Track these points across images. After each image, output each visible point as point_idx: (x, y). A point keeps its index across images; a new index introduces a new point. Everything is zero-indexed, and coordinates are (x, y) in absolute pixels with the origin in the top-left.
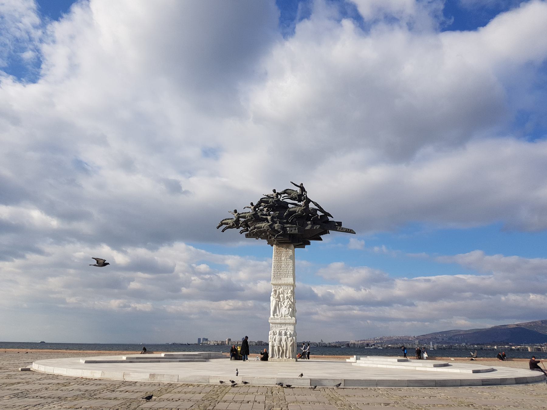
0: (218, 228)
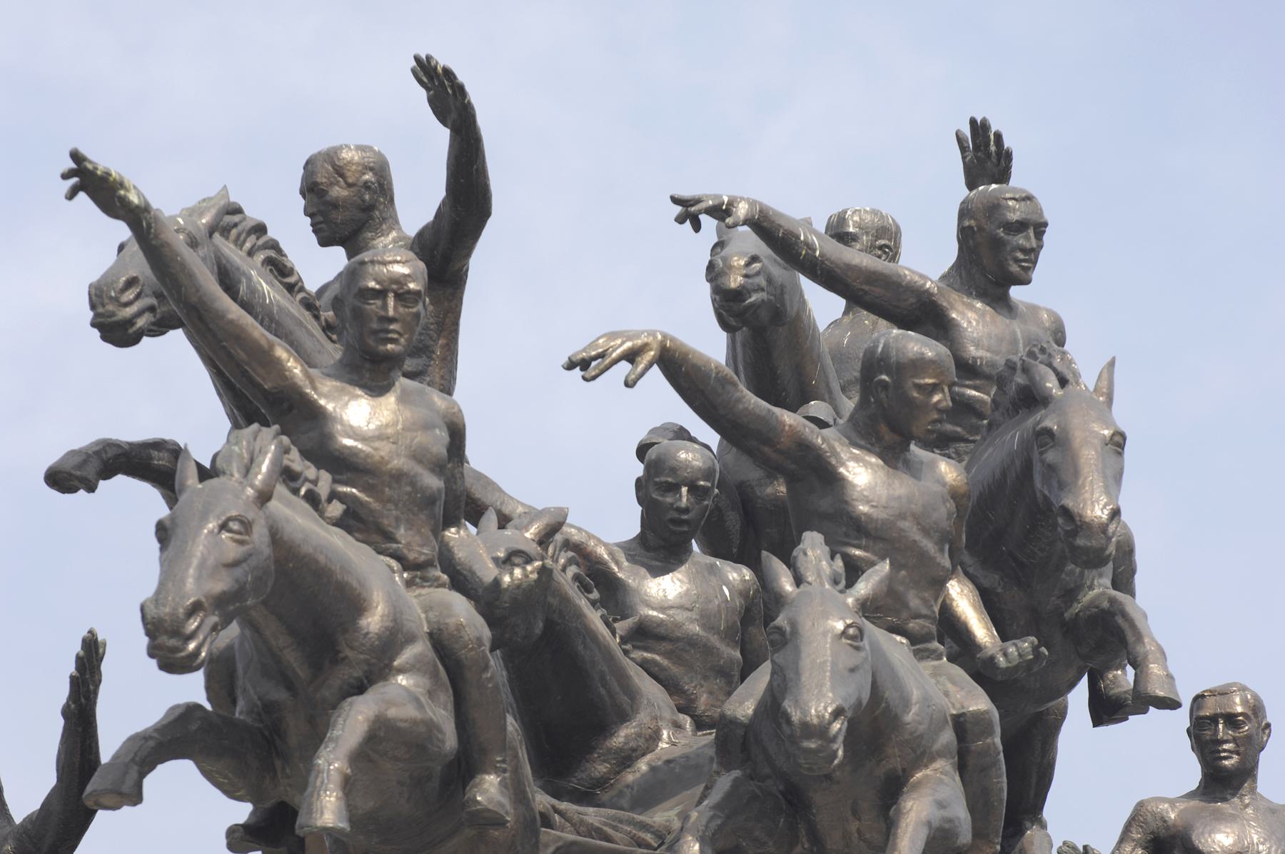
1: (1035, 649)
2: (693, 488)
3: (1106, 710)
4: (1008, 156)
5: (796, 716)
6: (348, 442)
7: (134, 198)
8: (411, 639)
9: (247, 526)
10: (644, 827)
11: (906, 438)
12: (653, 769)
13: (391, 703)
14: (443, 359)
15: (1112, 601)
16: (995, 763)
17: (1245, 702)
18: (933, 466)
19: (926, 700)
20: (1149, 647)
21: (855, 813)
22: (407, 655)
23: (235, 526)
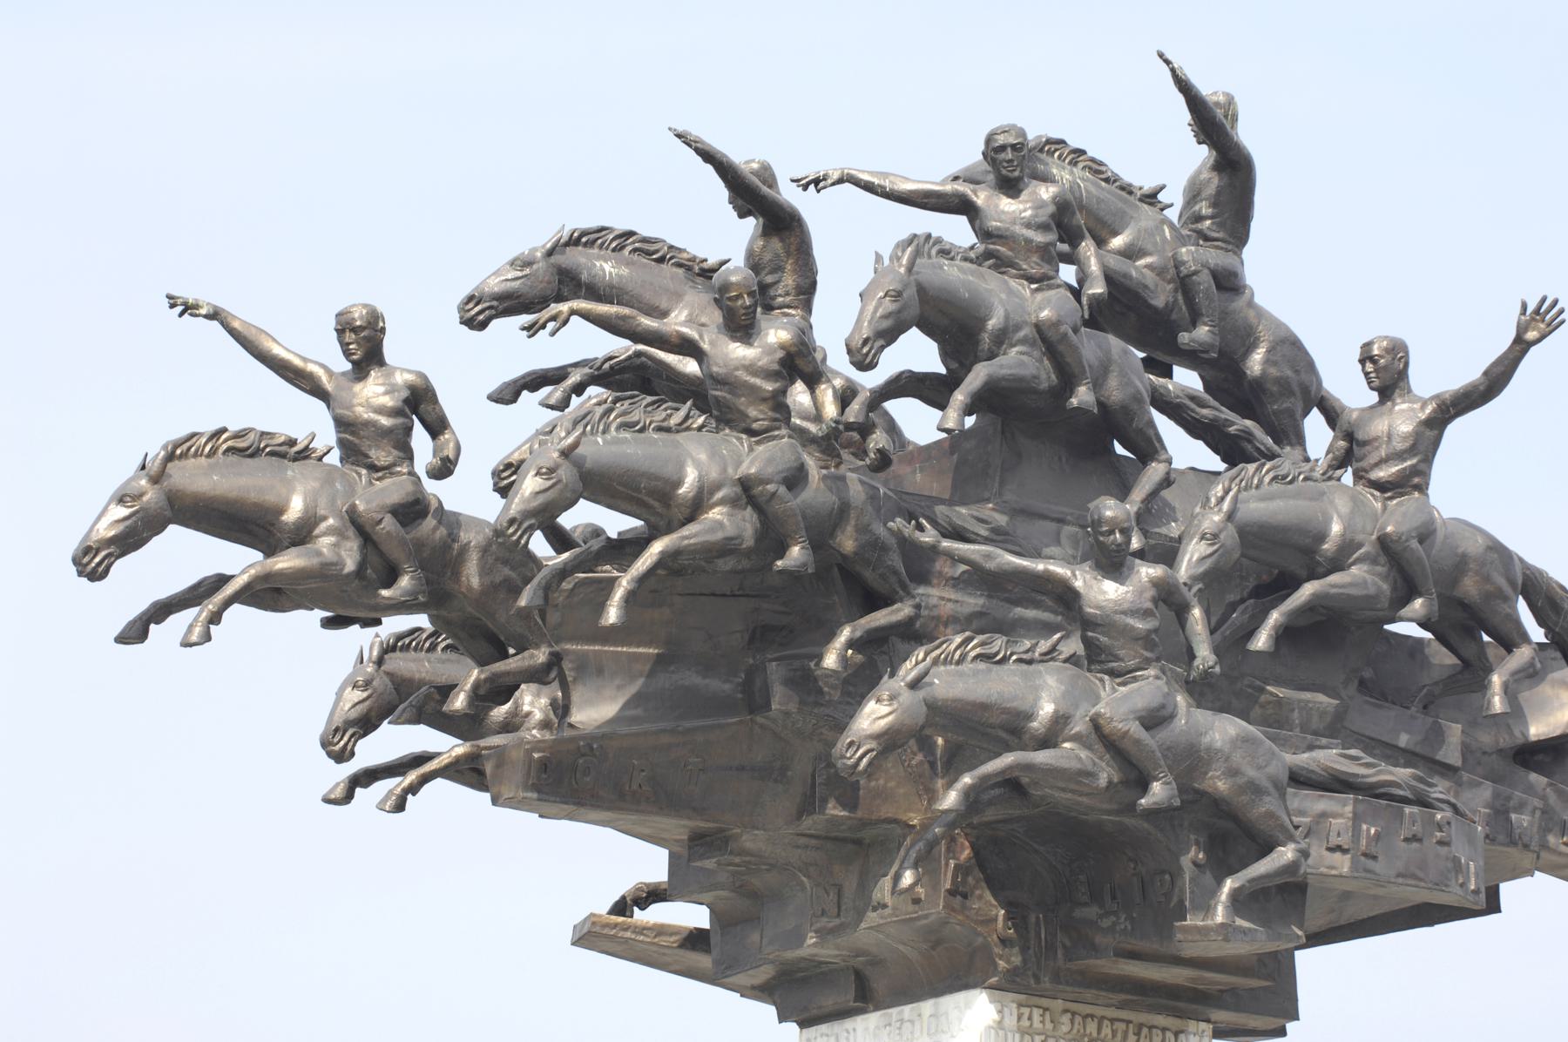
0: (93, 562)
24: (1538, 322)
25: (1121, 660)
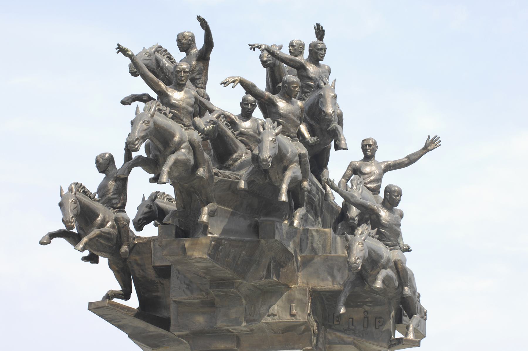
1: (317, 139)
2: (251, 104)
3: (337, 148)
4: (324, 31)
5: (261, 157)
6: (174, 101)
7: (130, 53)
8: (184, 142)
9: (148, 122)
10: (238, 175)
11: (291, 97)
12: (241, 162)
13: (179, 156)
14: (205, 75)
15: (336, 127)
16: (307, 163)
17: (372, 142)
18: (296, 102)
19: (292, 151)
20: (342, 137)
21: (278, 174)
22: (184, 145)
23: (146, 122)
24: (431, 144)
25: (392, 241)
